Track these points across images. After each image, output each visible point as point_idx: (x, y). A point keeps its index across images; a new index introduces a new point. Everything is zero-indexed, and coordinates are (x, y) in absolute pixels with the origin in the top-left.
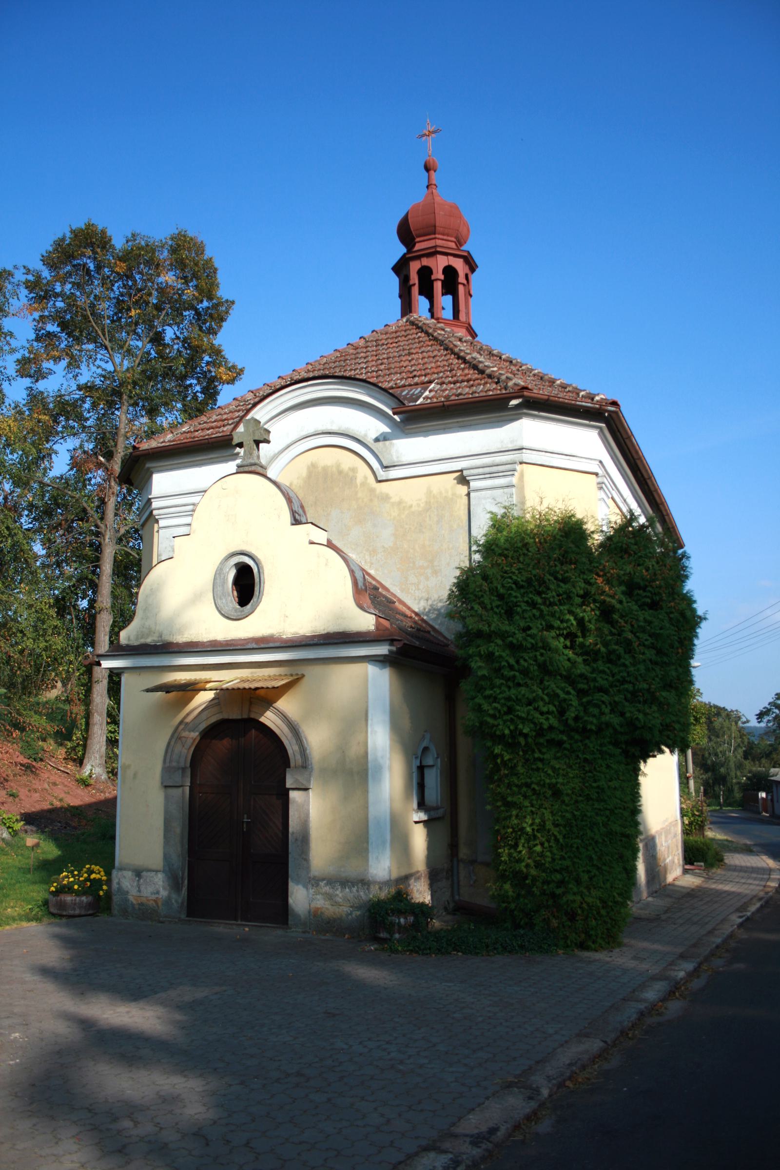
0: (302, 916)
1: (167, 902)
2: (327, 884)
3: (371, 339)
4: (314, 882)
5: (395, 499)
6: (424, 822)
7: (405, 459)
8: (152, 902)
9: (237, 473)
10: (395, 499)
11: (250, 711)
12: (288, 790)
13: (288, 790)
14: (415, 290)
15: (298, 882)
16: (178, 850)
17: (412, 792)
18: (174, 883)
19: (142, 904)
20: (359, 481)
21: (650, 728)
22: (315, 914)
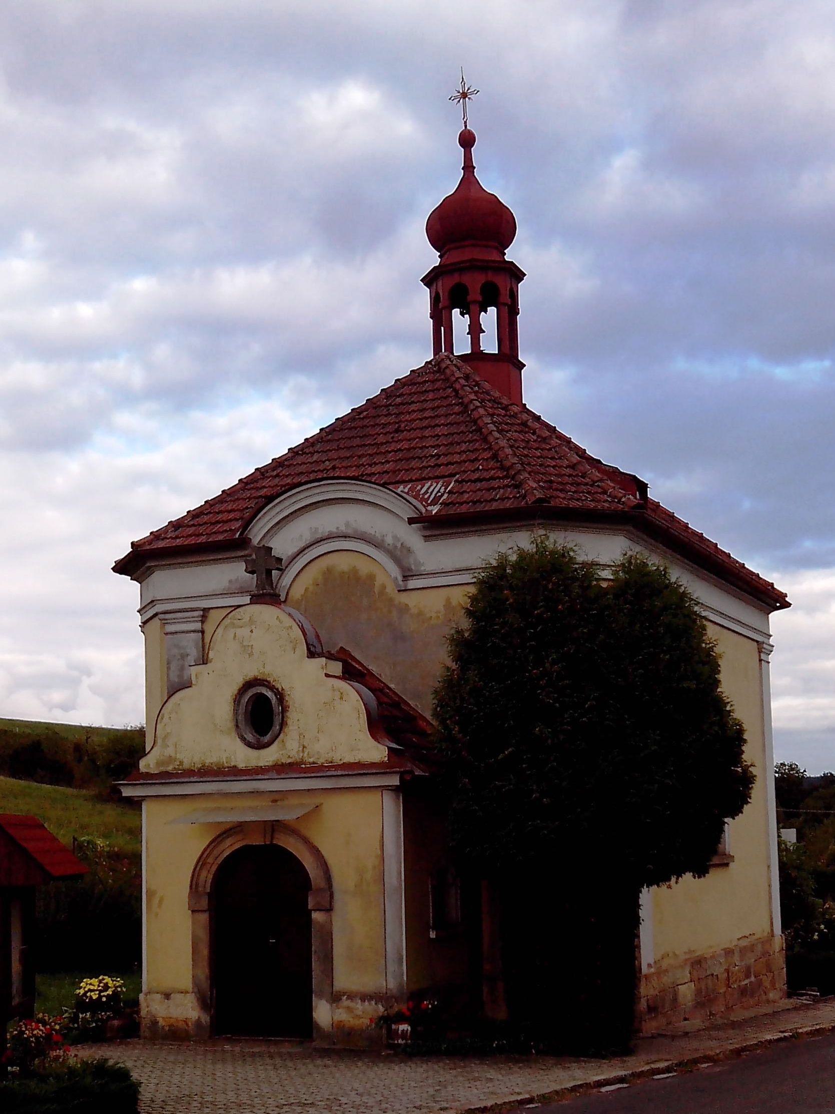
0: (326, 1030)
1: (198, 1023)
2: (347, 999)
3: (761, 999)
4: (335, 998)
5: (414, 611)
6: (395, 790)
7: (429, 567)
8: (181, 1023)
9: (251, 603)
10: (414, 611)
11: (272, 838)
12: (311, 911)
13: (311, 911)
14: (654, 561)
15: (321, 996)
16: (204, 972)
17: (399, 799)
18: (204, 1003)
19: (171, 1026)
20: (376, 590)
21: (711, 957)
22: (339, 1027)
